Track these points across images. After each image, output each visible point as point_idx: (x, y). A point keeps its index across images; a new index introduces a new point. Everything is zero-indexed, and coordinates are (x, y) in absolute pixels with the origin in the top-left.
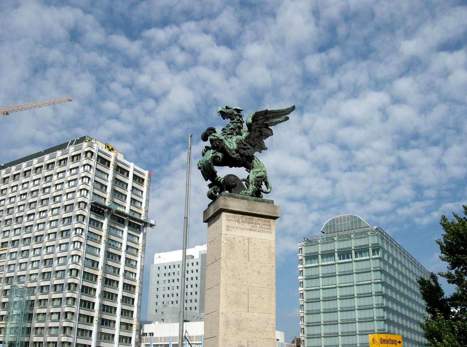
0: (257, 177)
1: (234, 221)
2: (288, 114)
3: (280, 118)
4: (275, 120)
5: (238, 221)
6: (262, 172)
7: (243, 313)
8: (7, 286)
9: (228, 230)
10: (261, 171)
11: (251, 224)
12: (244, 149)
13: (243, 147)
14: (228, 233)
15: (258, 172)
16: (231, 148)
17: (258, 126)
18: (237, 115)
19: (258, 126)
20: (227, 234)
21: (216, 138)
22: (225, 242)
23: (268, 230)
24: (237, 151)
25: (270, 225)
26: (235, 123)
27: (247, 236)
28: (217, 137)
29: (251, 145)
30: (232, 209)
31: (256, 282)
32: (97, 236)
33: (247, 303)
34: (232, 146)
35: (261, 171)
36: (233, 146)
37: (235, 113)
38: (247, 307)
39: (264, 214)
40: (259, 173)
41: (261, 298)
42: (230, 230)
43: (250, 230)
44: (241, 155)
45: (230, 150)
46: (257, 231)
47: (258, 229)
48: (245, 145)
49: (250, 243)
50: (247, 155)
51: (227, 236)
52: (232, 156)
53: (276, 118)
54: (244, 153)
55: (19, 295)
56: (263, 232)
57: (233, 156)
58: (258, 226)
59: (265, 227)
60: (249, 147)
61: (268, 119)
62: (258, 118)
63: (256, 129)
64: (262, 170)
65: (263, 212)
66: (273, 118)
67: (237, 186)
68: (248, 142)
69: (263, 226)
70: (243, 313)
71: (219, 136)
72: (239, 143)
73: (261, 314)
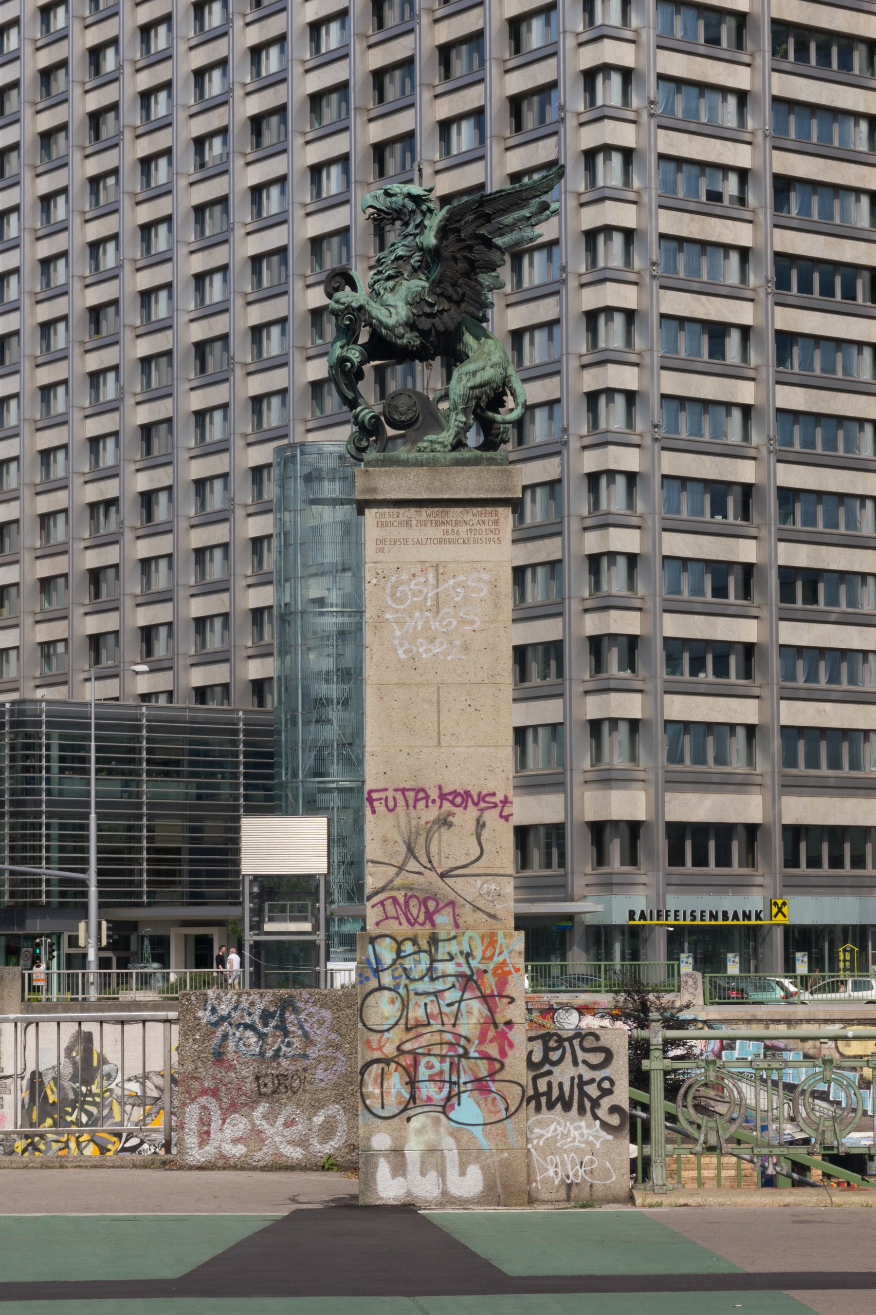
0: (472, 388)
1: (396, 524)
2: (547, 192)
3: (521, 208)
4: (508, 219)
5: (408, 524)
6: (488, 368)
7: (424, 750)
8: (97, 550)
9: (382, 551)
10: (483, 369)
11: (444, 527)
12: (429, 315)
13: (427, 310)
14: (381, 557)
15: (474, 374)
16: (391, 322)
17: (462, 244)
18: (413, 212)
19: (462, 244)
20: (379, 559)
21: (342, 307)
22: (374, 581)
23: (492, 536)
24: (411, 325)
25: (496, 522)
26: (411, 238)
27: (431, 559)
28: (343, 304)
29: (449, 299)
30: (388, 496)
31: (459, 672)
32: (718, 97)
33: (436, 724)
34: (393, 315)
35: (483, 369)
36: (397, 314)
37: (411, 205)
38: (435, 734)
39: (474, 496)
40: (479, 374)
41: (472, 709)
42: (386, 549)
43: (440, 541)
44: (424, 334)
45: (387, 327)
46: (461, 541)
47: (464, 535)
48: (431, 305)
49: (440, 576)
50: (441, 328)
51: (379, 565)
52: (396, 344)
53: (515, 210)
54: (433, 325)
55: (286, 737)
56: (476, 541)
57: (399, 342)
58: (463, 529)
59: (483, 528)
60: (446, 306)
61: (488, 219)
62: (460, 220)
63: (458, 256)
64: (490, 363)
65: (473, 492)
66: (505, 211)
67: (421, 419)
68: (442, 295)
69: (478, 527)
70: (424, 750)
71: (350, 299)
72: (415, 302)
73: (471, 749)
